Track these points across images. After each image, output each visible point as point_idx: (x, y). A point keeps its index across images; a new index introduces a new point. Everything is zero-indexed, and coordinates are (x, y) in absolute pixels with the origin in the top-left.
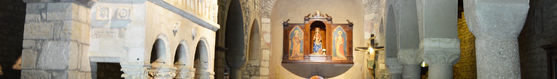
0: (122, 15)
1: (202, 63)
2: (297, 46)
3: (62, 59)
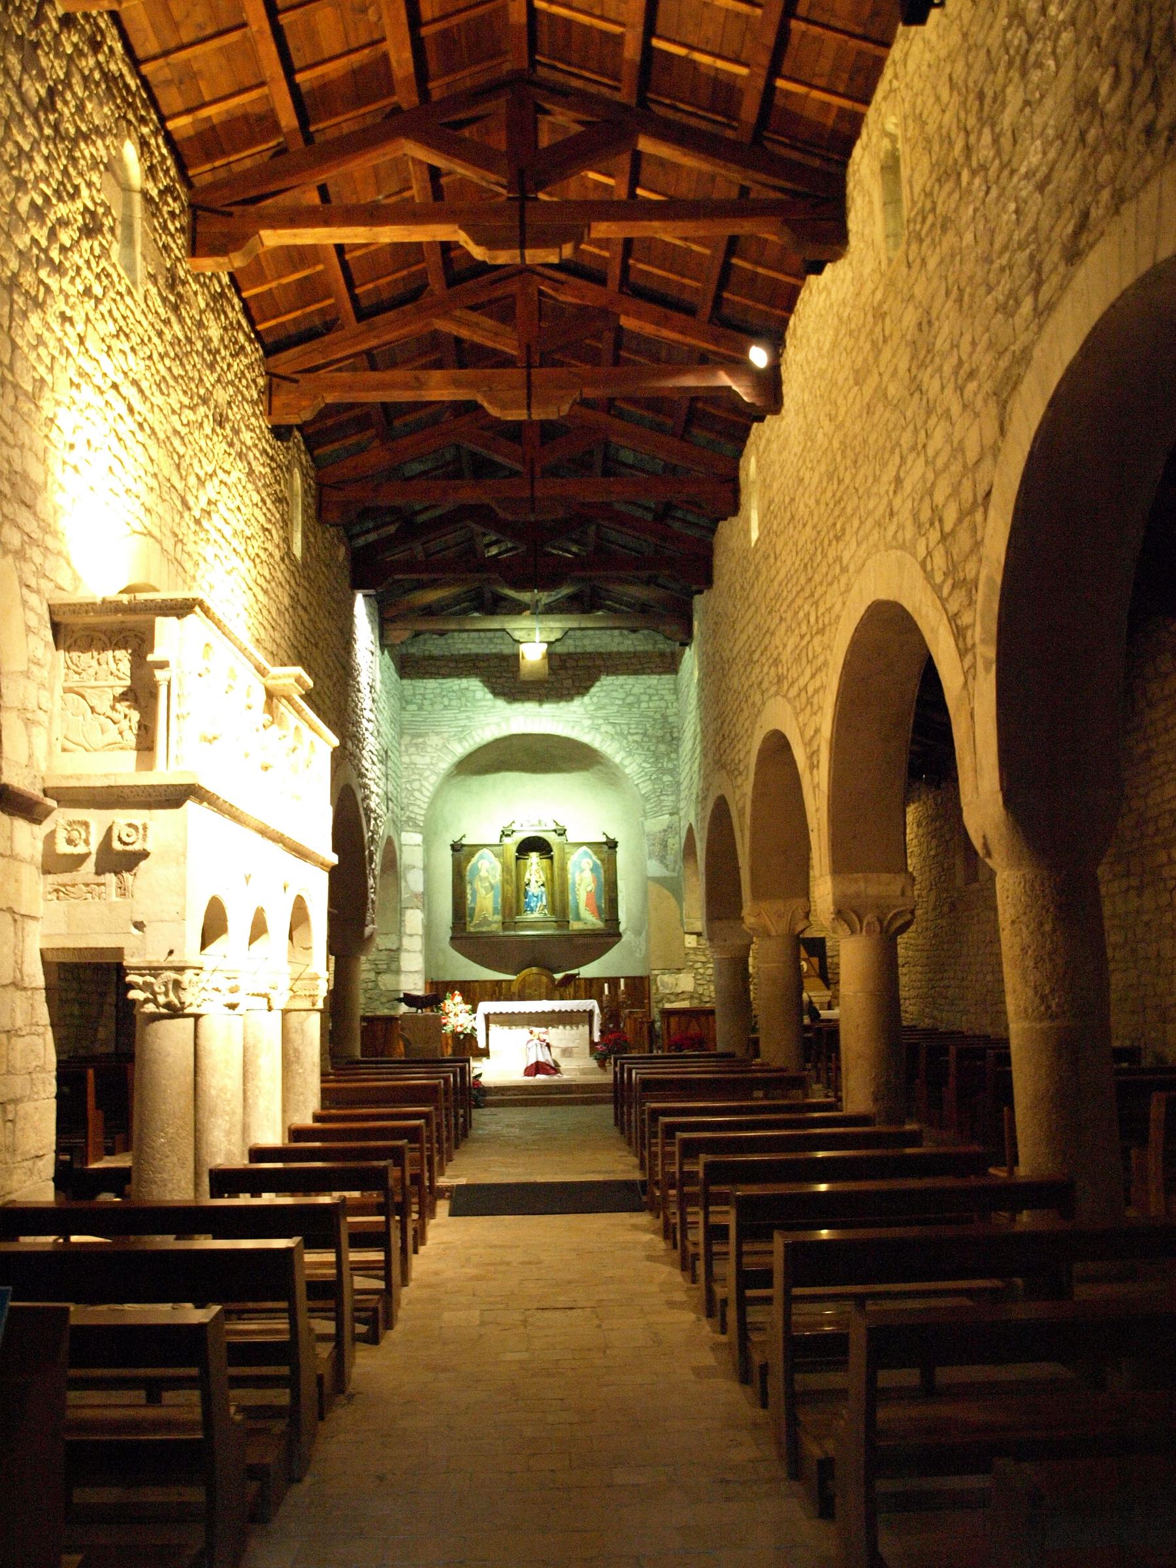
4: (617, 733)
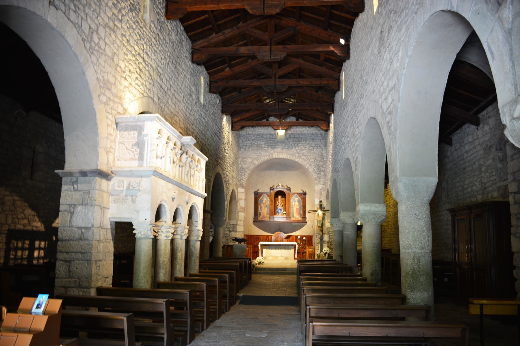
0: (133, 186)
1: (194, 222)
4: (306, 159)
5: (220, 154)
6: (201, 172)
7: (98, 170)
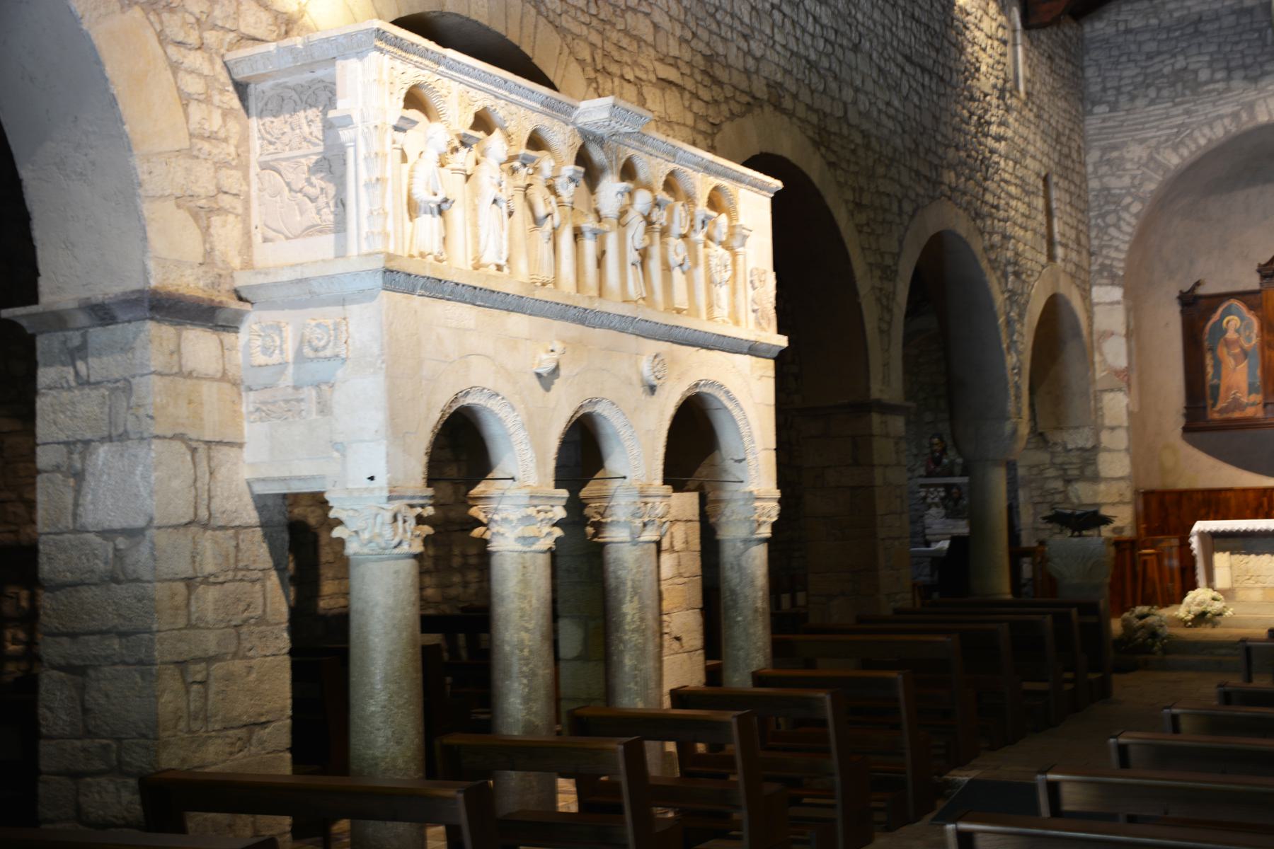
0: (315, 343)
1: (729, 464)
2: (1234, 369)
3: (136, 495)
5: (948, 146)
6: (743, 245)
7: (155, 292)
